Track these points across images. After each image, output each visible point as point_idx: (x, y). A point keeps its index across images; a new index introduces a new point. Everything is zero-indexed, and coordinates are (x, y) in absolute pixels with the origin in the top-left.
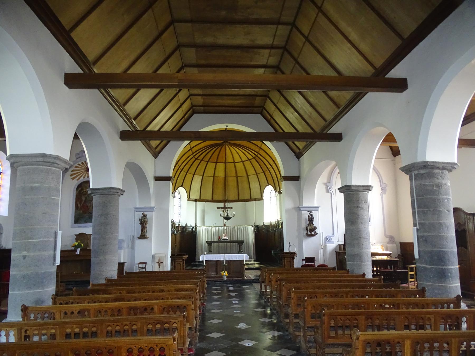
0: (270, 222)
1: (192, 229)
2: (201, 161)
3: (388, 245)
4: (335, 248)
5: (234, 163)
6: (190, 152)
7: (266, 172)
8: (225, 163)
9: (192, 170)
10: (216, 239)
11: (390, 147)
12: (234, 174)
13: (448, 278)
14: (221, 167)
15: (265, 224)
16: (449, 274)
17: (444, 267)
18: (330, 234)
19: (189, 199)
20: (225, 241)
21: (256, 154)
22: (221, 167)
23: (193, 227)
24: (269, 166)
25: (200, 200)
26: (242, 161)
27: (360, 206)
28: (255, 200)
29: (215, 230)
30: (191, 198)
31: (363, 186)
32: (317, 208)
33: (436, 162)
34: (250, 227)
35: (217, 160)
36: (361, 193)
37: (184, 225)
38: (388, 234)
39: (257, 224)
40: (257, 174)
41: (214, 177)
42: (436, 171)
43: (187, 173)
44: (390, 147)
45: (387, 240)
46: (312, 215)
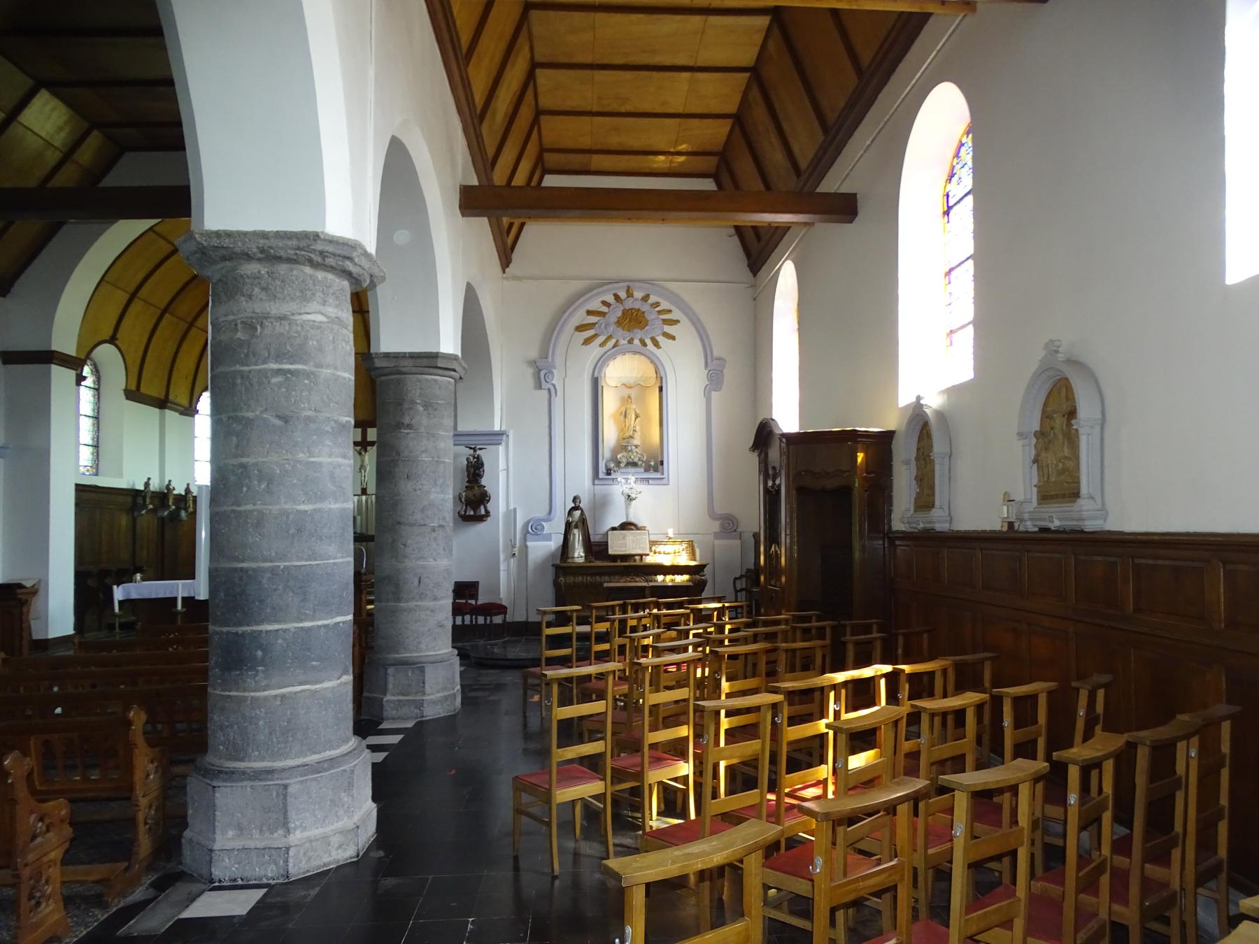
3: (717, 542)
4: (553, 555)
11: (739, 230)
13: (253, 668)
16: (259, 653)
17: (240, 629)
18: (542, 513)
27: (406, 420)
30: (459, 429)
31: (413, 356)
32: (497, 437)
33: (229, 234)
36: (411, 380)
38: (719, 510)
42: (250, 268)
44: (739, 230)
45: (716, 526)
46: (478, 458)
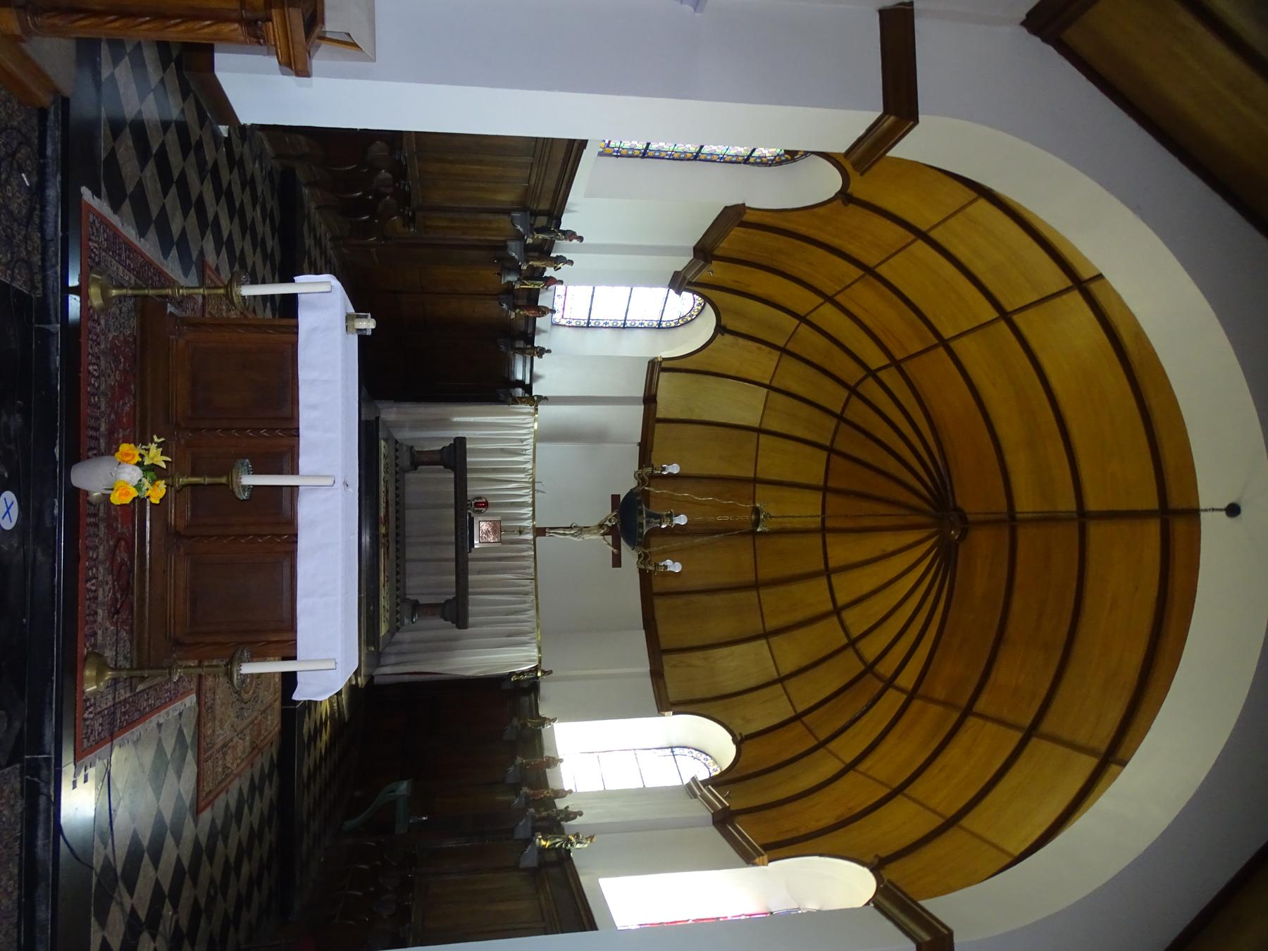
0: (561, 754)
1: (521, 384)
2: (840, 418)
5: (828, 572)
6: (908, 339)
7: (798, 728)
8: (824, 530)
9: (796, 378)
10: (474, 490)
12: (767, 572)
14: (805, 510)
15: (545, 730)
19: (656, 367)
20: (464, 531)
21: (907, 679)
22: (805, 510)
23: (528, 389)
24: (849, 747)
25: (651, 420)
26: (837, 611)
28: (657, 674)
29: (515, 488)
30: (663, 376)
34: (534, 653)
35: (837, 492)
37: (539, 341)
39: (546, 688)
40: (781, 680)
41: (755, 481)
43: (784, 351)
